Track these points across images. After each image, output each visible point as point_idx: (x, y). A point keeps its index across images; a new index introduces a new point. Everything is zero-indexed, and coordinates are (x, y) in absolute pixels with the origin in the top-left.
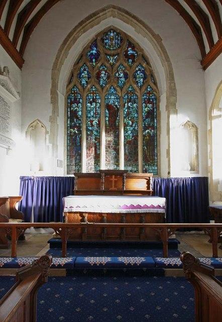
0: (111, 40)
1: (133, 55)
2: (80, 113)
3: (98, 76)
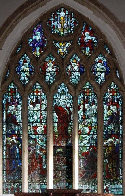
0: (62, 22)
1: (91, 42)
2: (19, 118)
3: (44, 71)
